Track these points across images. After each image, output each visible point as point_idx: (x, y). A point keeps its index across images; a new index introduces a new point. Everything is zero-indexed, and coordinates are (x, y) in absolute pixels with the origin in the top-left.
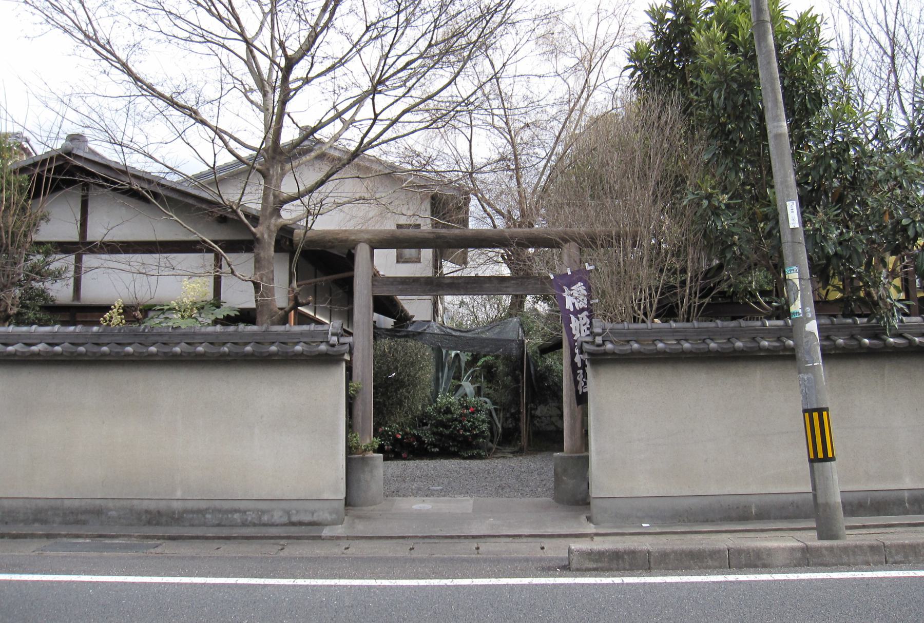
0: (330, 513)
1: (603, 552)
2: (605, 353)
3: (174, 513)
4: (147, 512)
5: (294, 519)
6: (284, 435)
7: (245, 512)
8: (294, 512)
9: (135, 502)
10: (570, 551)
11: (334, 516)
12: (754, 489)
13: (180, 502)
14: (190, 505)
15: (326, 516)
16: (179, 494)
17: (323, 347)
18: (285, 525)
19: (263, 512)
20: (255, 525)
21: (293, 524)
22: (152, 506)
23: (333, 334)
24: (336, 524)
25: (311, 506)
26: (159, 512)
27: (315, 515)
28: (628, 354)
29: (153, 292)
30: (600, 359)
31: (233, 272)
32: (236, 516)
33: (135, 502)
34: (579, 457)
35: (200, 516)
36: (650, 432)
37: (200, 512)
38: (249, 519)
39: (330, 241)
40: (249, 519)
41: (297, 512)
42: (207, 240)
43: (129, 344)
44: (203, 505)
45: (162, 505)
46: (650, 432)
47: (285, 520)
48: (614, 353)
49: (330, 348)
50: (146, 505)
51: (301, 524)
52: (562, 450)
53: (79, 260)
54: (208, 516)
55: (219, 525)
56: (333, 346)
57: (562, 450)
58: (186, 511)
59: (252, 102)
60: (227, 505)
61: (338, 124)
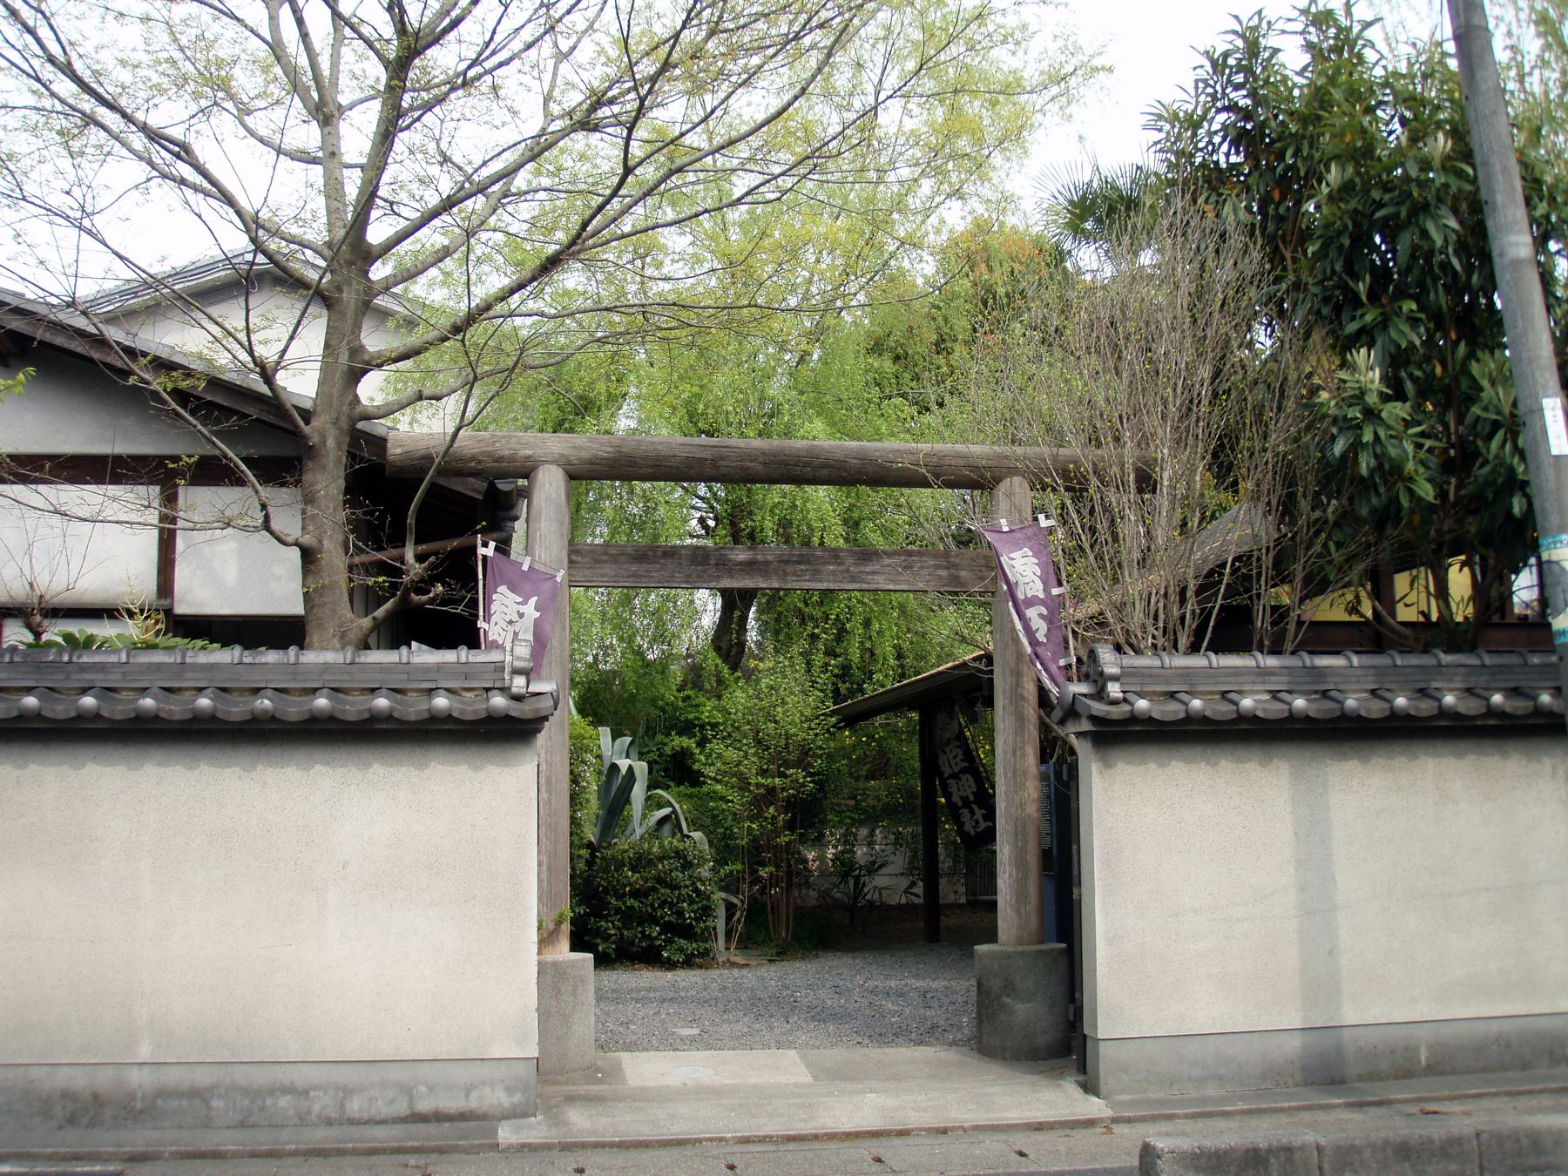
0: (510, 1091)
1: (1226, 1152)
2: (1133, 718)
3: (132, 1097)
4: (67, 1095)
5: (424, 1106)
6: (384, 908)
7: (305, 1093)
8: (423, 1089)
9: (35, 1072)
10: (1147, 1152)
11: (517, 1098)
12: (1424, 1011)
13: (146, 1071)
14: (172, 1077)
15: (495, 1098)
16: (145, 1052)
17: (498, 701)
18: (403, 1120)
19: (348, 1092)
20: (329, 1122)
21: (418, 1118)
22: (78, 1081)
23: (516, 672)
24: (525, 1115)
25: (462, 1074)
26: (96, 1096)
27: (474, 1095)
28: (72, 719)
29: (74, 567)
30: (1125, 734)
31: (267, 525)
32: (285, 1102)
33: (35, 1072)
34: (1041, 952)
35: (197, 1102)
36: (1217, 895)
37: (195, 1093)
38: (316, 1108)
39: (473, 458)
40: (316, 1108)
41: (431, 1089)
42: (231, 454)
43: (29, 690)
44: (204, 1077)
45: (103, 1080)
46: (1217, 895)
47: (402, 1108)
48: (1150, 720)
49: (513, 704)
50: (63, 1079)
51: (439, 1117)
52: (992, 937)
53: (170, 499)
54: (217, 1103)
55: (242, 1125)
56: (518, 698)
57: (992, 937)
58: (163, 1093)
59: (252, 134)
60: (260, 1077)
61: (479, 202)
